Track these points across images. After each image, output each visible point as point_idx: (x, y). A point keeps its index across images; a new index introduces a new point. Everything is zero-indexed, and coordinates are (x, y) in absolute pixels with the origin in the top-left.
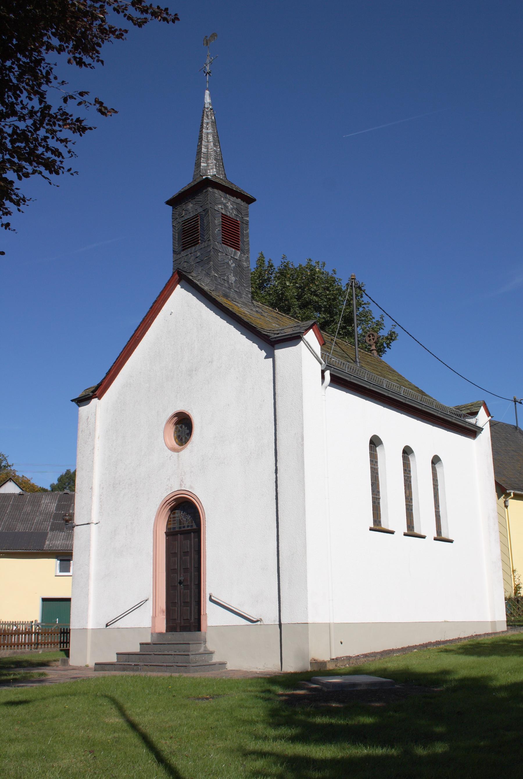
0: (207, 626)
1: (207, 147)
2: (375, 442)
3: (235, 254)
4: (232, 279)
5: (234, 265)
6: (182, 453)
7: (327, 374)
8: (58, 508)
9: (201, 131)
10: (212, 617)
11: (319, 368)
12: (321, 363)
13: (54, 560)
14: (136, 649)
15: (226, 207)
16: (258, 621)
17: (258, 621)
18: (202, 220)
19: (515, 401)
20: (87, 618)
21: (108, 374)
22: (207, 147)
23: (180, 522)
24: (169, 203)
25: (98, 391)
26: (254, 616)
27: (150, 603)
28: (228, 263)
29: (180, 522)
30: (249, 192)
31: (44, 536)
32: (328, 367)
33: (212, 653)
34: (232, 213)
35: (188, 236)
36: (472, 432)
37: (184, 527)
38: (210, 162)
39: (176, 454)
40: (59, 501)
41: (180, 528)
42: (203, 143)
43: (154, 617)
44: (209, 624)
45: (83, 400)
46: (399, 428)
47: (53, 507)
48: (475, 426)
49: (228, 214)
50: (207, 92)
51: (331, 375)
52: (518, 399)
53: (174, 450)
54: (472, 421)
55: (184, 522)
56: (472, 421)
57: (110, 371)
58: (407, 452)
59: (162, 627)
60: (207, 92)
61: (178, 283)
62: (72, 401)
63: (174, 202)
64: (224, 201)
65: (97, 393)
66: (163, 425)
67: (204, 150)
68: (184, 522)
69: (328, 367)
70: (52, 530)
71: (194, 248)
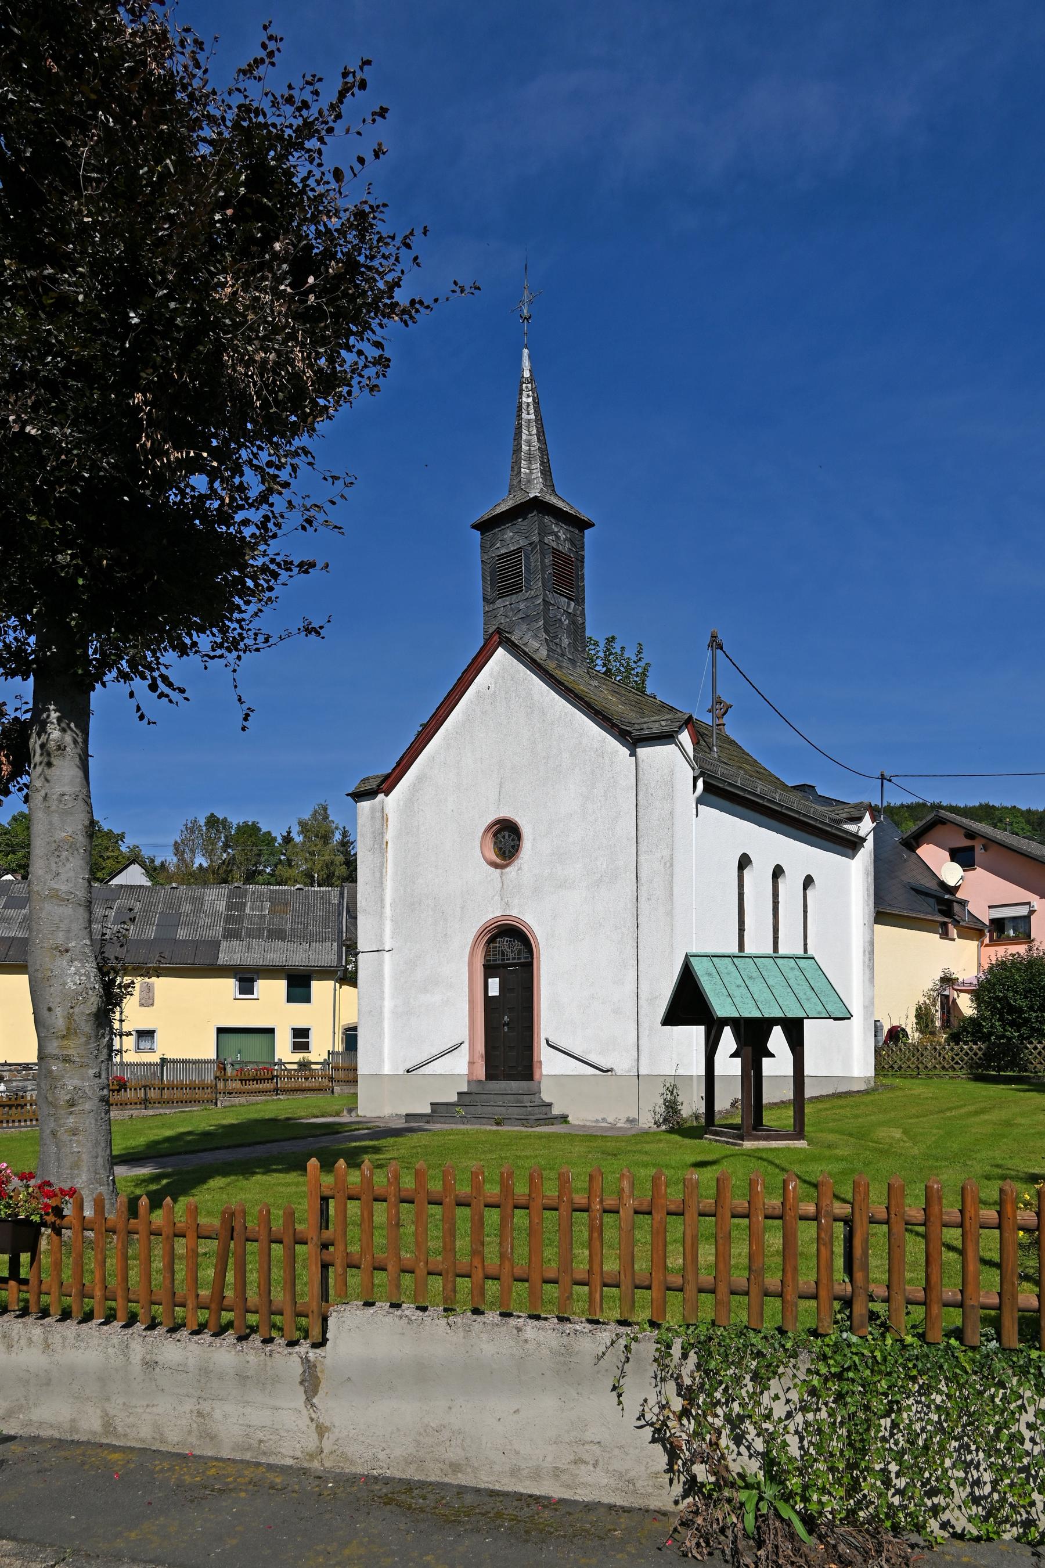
0: (541, 1074)
1: (529, 443)
2: (744, 862)
3: (569, 605)
4: (566, 641)
5: (567, 622)
6: (508, 869)
7: (700, 783)
8: (230, 906)
9: (519, 416)
10: (550, 1064)
11: (690, 774)
12: (693, 769)
13: (233, 981)
14: (454, 1098)
15: (558, 537)
16: (608, 1071)
17: (608, 1071)
18: (527, 557)
19: (883, 777)
20: (381, 1058)
21: (398, 764)
22: (529, 443)
23: (503, 954)
24: (476, 527)
25: (387, 784)
26: (605, 1065)
27: (465, 1047)
28: (560, 620)
29: (503, 954)
30: (585, 515)
31: (216, 945)
32: (702, 774)
33: (550, 1105)
34: (565, 548)
35: (504, 579)
36: (850, 845)
37: (508, 959)
38: (534, 466)
39: (498, 871)
40: (229, 897)
41: (503, 960)
42: (524, 437)
43: (471, 1063)
44: (544, 1072)
45: (359, 796)
46: (770, 845)
47: (221, 906)
48: (856, 836)
49: (561, 548)
50: (526, 351)
51: (704, 782)
52: (887, 774)
53: (495, 865)
54: (851, 827)
55: (509, 956)
56: (851, 827)
57: (402, 759)
58: (778, 872)
59: (481, 1073)
60: (526, 351)
61: (499, 644)
62: (348, 795)
63: (484, 527)
64: (556, 530)
65: (384, 786)
66: (480, 835)
67: (525, 448)
68: (509, 956)
69: (702, 774)
70: (225, 937)
71: (514, 596)
